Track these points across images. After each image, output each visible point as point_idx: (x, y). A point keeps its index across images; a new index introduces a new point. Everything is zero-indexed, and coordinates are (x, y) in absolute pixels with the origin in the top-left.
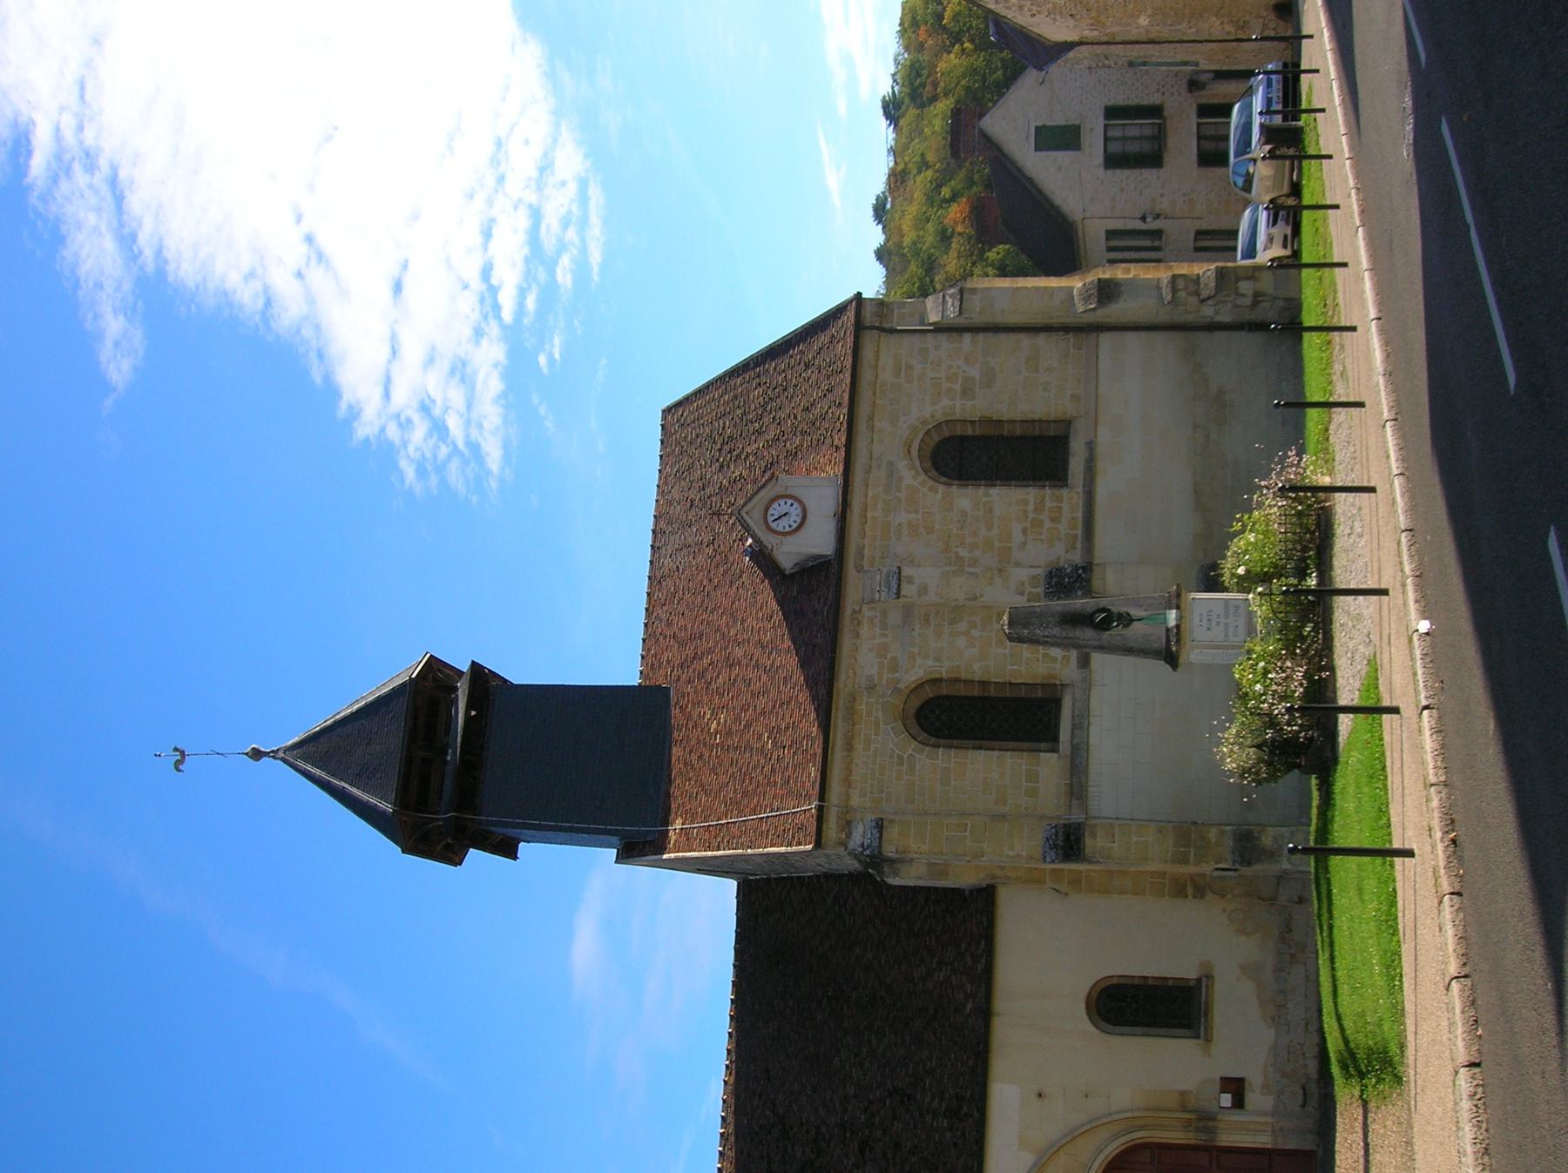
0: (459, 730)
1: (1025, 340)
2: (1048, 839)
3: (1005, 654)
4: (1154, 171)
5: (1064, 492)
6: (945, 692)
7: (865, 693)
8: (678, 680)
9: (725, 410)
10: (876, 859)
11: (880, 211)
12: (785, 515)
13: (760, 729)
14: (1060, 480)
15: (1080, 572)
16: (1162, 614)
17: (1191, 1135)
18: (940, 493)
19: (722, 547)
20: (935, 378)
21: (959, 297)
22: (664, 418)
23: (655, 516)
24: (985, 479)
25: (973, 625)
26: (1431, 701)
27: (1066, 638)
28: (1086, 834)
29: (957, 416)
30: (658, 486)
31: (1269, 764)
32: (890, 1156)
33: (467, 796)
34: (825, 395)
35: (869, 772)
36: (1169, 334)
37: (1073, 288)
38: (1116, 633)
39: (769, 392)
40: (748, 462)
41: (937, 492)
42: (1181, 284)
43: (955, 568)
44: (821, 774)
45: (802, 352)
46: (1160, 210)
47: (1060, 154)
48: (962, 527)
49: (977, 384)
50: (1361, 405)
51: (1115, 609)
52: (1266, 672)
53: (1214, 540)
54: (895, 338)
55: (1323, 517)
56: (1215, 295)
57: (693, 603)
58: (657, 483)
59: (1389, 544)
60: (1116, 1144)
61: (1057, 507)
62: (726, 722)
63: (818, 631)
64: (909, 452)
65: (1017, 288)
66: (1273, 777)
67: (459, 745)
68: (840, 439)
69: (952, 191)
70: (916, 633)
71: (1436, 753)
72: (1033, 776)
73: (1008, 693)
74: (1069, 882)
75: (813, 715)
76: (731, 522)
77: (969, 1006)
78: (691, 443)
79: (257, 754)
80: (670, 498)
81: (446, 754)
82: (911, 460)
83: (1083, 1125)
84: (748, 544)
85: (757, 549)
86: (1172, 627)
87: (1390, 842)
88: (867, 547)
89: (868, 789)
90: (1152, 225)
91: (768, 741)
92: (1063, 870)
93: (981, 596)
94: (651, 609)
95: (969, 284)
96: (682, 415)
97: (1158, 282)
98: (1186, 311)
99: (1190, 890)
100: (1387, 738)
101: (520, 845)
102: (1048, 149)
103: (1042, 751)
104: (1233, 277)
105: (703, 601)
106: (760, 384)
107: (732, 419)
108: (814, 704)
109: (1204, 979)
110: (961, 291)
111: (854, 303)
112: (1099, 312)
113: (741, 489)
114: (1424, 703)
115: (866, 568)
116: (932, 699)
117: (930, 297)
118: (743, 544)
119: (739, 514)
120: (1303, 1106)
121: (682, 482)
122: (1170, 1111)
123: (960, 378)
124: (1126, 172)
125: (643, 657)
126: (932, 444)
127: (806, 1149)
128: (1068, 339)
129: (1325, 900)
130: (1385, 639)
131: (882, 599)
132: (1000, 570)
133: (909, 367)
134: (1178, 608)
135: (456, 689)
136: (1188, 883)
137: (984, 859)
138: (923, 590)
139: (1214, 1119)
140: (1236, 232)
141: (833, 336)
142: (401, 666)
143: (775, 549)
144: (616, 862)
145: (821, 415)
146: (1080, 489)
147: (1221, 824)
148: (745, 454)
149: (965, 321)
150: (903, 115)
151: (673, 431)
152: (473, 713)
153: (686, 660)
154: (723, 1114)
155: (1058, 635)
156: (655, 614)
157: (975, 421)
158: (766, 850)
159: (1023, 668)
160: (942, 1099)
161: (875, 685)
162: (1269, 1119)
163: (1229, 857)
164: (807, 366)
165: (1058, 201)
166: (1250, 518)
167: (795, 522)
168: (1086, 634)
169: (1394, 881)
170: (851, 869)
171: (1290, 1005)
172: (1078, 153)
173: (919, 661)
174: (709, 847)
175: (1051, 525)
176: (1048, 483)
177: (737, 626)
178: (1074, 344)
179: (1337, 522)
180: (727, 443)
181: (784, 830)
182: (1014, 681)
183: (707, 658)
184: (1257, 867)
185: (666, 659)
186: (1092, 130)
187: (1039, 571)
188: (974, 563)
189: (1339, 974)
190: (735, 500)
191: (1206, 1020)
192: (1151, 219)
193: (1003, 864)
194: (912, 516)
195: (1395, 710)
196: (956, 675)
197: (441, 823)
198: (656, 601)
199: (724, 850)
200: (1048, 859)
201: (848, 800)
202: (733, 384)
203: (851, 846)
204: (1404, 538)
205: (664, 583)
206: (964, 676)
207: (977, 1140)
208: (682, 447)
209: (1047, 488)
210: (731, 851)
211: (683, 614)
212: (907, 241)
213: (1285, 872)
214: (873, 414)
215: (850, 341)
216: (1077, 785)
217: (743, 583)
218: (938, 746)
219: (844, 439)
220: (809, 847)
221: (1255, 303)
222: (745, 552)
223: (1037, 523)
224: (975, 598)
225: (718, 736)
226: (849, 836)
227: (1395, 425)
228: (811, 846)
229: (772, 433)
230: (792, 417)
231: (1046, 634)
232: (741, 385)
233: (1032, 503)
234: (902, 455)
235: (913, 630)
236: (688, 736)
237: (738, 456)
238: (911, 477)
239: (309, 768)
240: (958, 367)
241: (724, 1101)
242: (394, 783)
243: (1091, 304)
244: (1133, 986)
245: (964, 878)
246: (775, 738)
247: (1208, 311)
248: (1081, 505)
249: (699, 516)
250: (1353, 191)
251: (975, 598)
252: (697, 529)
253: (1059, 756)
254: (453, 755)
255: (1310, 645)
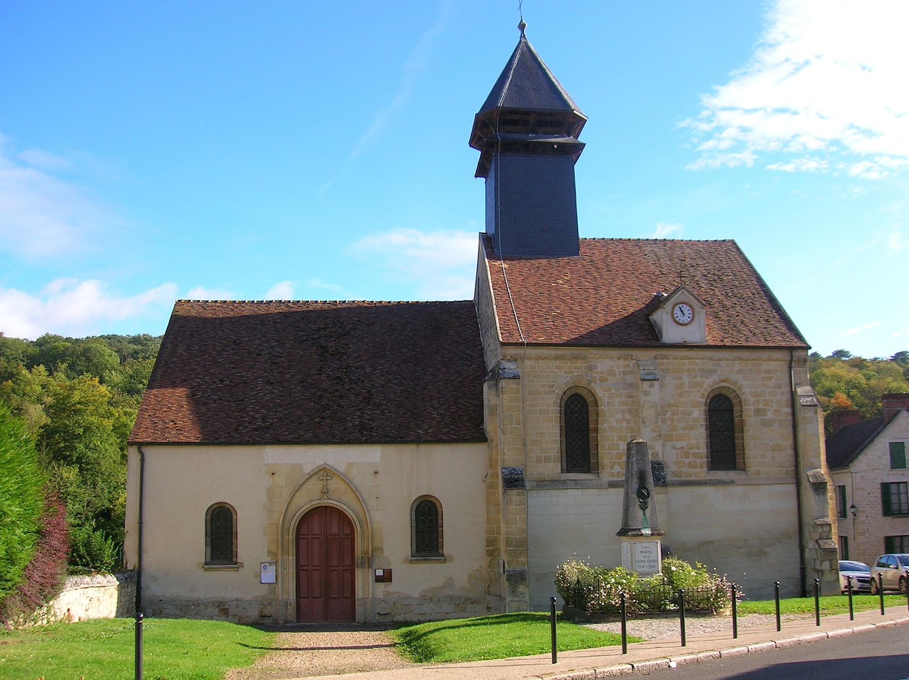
0: (546, 140)
1: (789, 442)
2: (514, 470)
3: (614, 441)
4: (881, 511)
5: (705, 469)
6: (590, 408)
7: (588, 365)
8: (584, 260)
9: (738, 275)
10: (497, 376)
11: (840, 354)
12: (683, 314)
13: (562, 307)
14: (711, 466)
15: (662, 480)
16: (648, 525)
17: (360, 554)
18: (701, 400)
19: (660, 279)
20: (765, 394)
21: (812, 404)
22: (729, 241)
23: (673, 240)
24: (710, 425)
25: (628, 422)
26: (636, 669)
27: (632, 474)
28: (519, 490)
29: (744, 407)
30: (690, 240)
31: (568, 588)
32: (335, 394)
33: (509, 147)
34: (751, 332)
35: (544, 369)
36: (797, 522)
37: (820, 468)
38: (636, 501)
39: (750, 300)
40: (709, 291)
41: (701, 398)
42: (826, 529)
43: (660, 410)
44: (541, 343)
45: (774, 317)
46: (859, 516)
47: (888, 457)
48: (682, 413)
49: (763, 417)
50: (779, 630)
51: (649, 500)
52: (621, 584)
53: (688, 553)
54: (786, 369)
55: (707, 612)
56: (821, 548)
57: (627, 265)
58: (692, 239)
59: (709, 645)
60: (353, 515)
61: (697, 466)
62: (564, 288)
63: (619, 336)
64: (723, 381)
65: (819, 437)
66: (561, 590)
67: (538, 140)
68: (727, 342)
69: (854, 396)
70: (622, 391)
71: (611, 672)
72: (547, 460)
73: (592, 444)
74: (492, 482)
75: (573, 337)
76: (675, 283)
77: (421, 432)
78: (716, 258)
79: (522, 27)
80: (684, 248)
81: (532, 134)
82: (719, 383)
83: (361, 496)
84: (664, 294)
85: (661, 299)
86: (641, 532)
87: (630, 642)
88: (668, 361)
89: (534, 370)
90: (849, 511)
91: (555, 312)
92: (498, 478)
93: (645, 426)
94: (622, 241)
95: (819, 410)
96: (732, 251)
97: (826, 516)
98: (811, 532)
99: (490, 548)
100: (606, 648)
101: (484, 178)
102: (891, 450)
103: (561, 464)
104: (831, 558)
105: (629, 271)
106: (754, 294)
107: (733, 280)
108: (579, 337)
109: (443, 558)
110: (815, 406)
111: (805, 345)
112: (807, 484)
113: (694, 288)
114: (635, 666)
115: (656, 361)
116: (586, 402)
117: (811, 388)
118: (663, 291)
119: (682, 288)
120: (379, 614)
121: (694, 254)
122: (372, 542)
123: (766, 408)
124: (879, 496)
125: (594, 239)
126: (728, 394)
127: (334, 348)
128: (791, 467)
129: (497, 620)
130: (658, 645)
131: (640, 371)
132: (660, 436)
133: (770, 378)
134: (652, 534)
135: (569, 136)
136: (495, 547)
137: (502, 435)
138: (647, 394)
139: (369, 567)
140: (848, 560)
141: (785, 334)
142: (578, 102)
143: (664, 309)
144: (480, 233)
145: (740, 331)
146: (707, 478)
147: (528, 563)
148: (714, 289)
149: (798, 408)
150: (898, 364)
151: (722, 246)
152: (556, 146)
153: (595, 263)
154: (347, 302)
155: (633, 470)
156: (619, 244)
157: (742, 417)
158: (496, 315)
159: (607, 451)
160: (369, 420)
161: (592, 370)
162: (370, 596)
163: (511, 569)
164: (767, 321)
165: (861, 457)
166: (704, 572)
167: (683, 321)
168: (635, 485)
169: (534, 654)
170: (488, 363)
171: (432, 604)
172: (889, 468)
173: (607, 394)
174: (494, 284)
175: (686, 464)
176: (710, 460)
177: (617, 290)
178: (788, 470)
179: (706, 619)
180: (719, 278)
181: (508, 325)
182: (599, 446)
183: (597, 275)
184: (506, 583)
185: (595, 252)
186: (904, 475)
187: (661, 455)
188: (663, 421)
189: (462, 629)
190: (687, 285)
191: (422, 560)
192: (853, 511)
193: (499, 445)
194: (687, 385)
195: (624, 652)
196: (600, 415)
197: (494, 134)
198: (626, 244)
199: (494, 293)
200: (504, 470)
201: (528, 359)
202: (752, 279)
203: (504, 362)
204: (716, 653)
205: (637, 248)
206: (600, 419)
207: (349, 440)
208: (714, 253)
209: (707, 459)
210: (493, 296)
211: (620, 260)
212: (825, 371)
213: (505, 599)
214: (743, 360)
215: (783, 344)
216: (544, 484)
217: (642, 292)
218: (560, 407)
219: (728, 344)
220: (501, 339)
221: (817, 571)
222: (658, 292)
223: (687, 455)
224: (644, 423)
225: (555, 285)
226: (509, 361)
227: (773, 647)
228: (502, 340)
229: (727, 303)
230: (738, 314)
231: (634, 463)
232: (752, 284)
233: (698, 452)
234: (721, 377)
235: (624, 389)
236: (553, 268)
237: (712, 285)
238: (709, 383)
239: (518, 57)
240: (772, 406)
241: (354, 302)
242: (515, 105)
243: (812, 479)
244: (437, 520)
245: (490, 425)
246: (558, 316)
247: (811, 545)
248: (698, 479)
249: (676, 265)
250: (894, 622)
251: (644, 423)
252: (668, 264)
253: (559, 474)
254: (532, 137)
255: (637, 607)
